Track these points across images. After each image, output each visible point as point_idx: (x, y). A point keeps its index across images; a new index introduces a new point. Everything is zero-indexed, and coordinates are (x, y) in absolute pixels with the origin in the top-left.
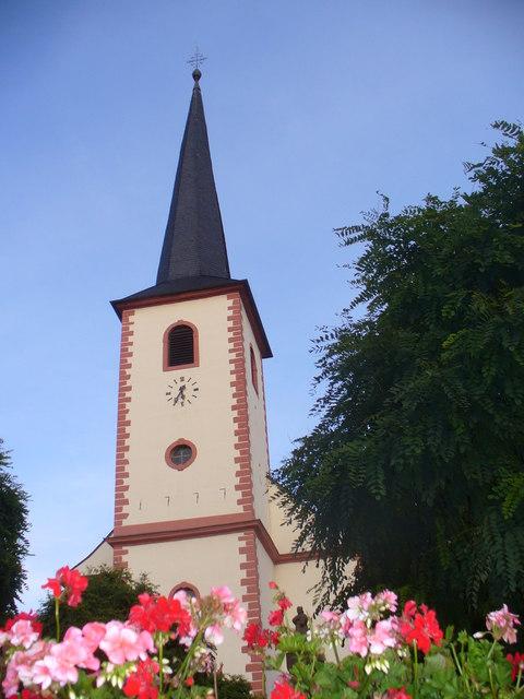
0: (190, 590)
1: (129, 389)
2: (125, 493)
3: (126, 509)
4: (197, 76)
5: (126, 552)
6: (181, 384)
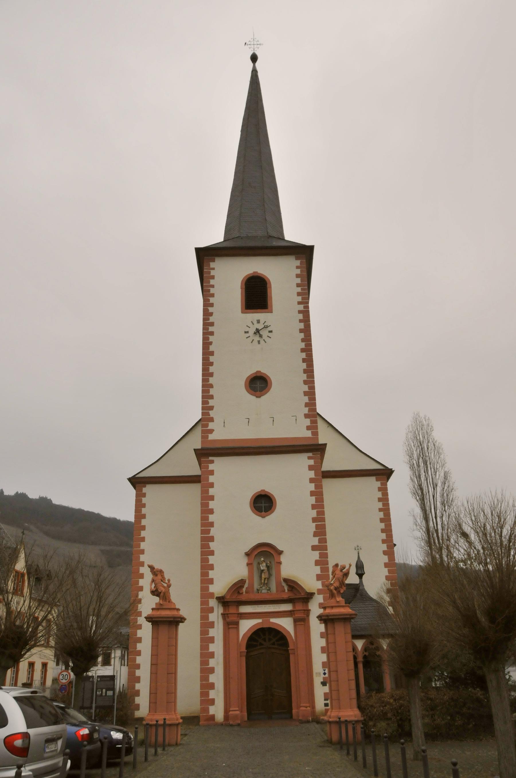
1: (212, 324)
4: (254, 58)
5: (212, 462)
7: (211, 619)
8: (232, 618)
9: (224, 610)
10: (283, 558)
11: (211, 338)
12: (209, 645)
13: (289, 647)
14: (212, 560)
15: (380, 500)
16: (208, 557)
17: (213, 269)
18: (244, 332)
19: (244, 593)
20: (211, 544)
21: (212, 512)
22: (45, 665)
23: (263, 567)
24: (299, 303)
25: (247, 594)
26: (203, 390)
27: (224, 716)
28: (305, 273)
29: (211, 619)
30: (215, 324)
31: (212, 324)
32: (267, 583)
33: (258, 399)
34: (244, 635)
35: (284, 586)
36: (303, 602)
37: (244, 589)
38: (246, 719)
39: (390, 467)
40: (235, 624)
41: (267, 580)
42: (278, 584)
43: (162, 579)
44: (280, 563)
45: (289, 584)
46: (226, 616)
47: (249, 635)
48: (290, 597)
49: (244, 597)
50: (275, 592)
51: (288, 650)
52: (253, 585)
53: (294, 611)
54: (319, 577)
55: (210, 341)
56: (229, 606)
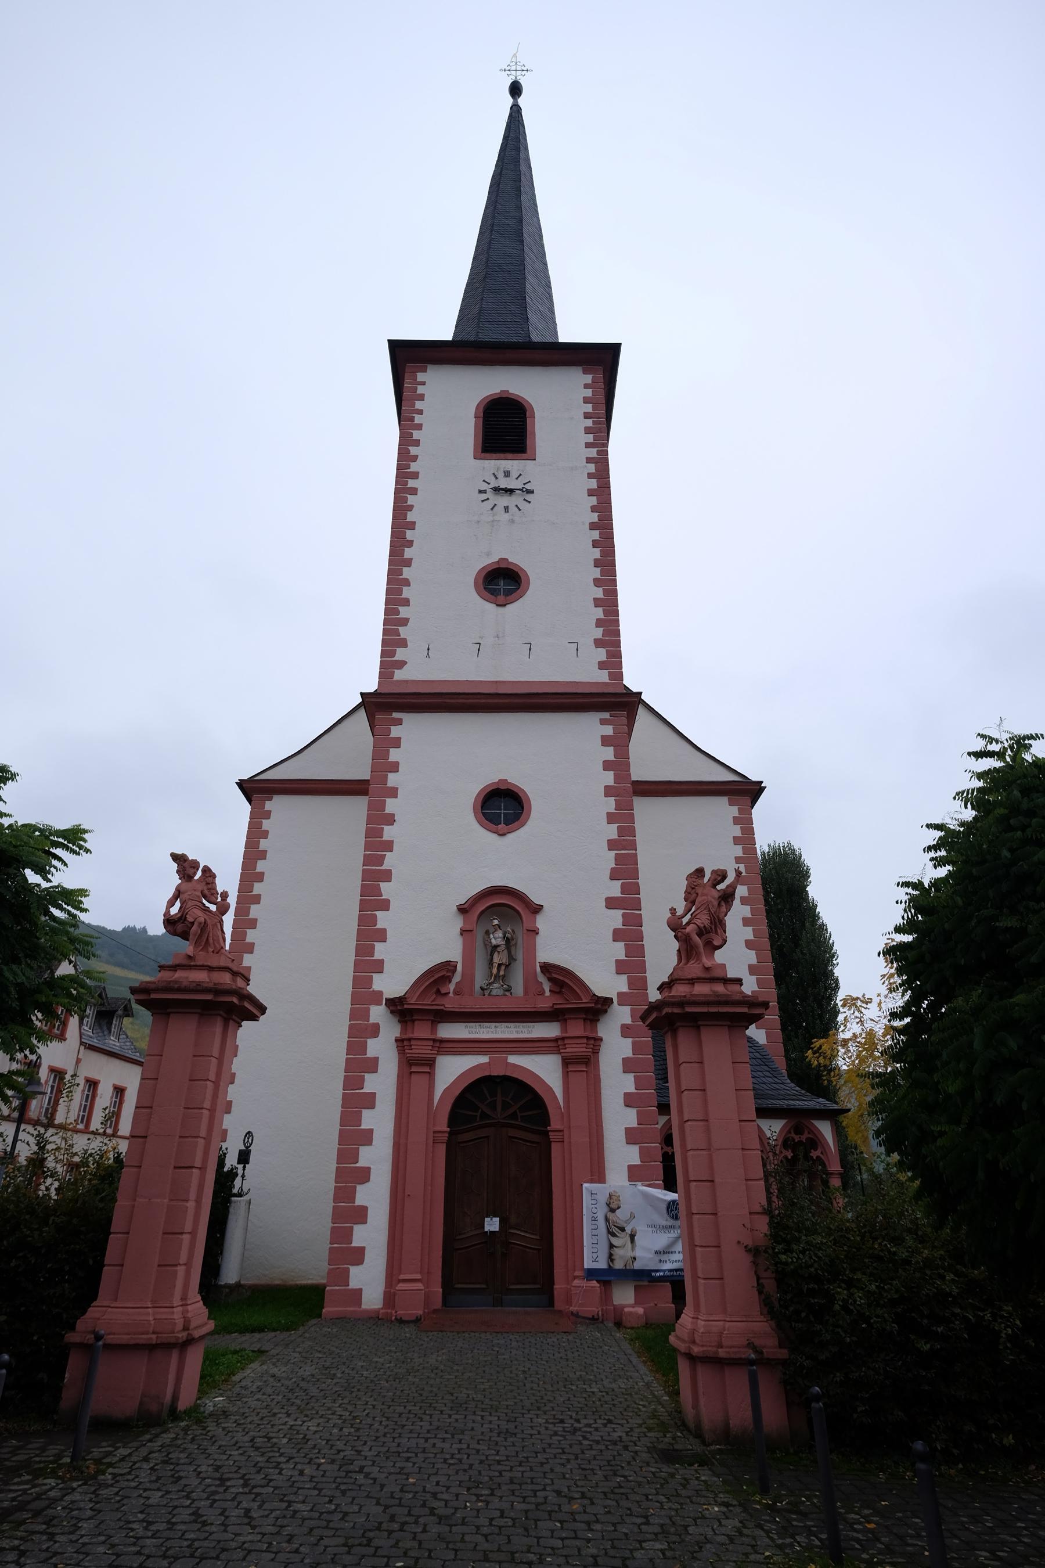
0: (105, 1109)
1: (415, 475)
2: (402, 630)
3: (400, 654)
4: (516, 90)
5: (399, 722)
6: (490, 494)
7: (371, 1053)
8: (419, 1050)
9: (404, 1030)
10: (541, 922)
11: (411, 499)
12: (361, 1112)
13: (550, 1126)
14: (383, 919)
15: (737, 841)
16: (375, 915)
17: (423, 383)
18: (477, 491)
19: (451, 994)
20: (383, 886)
21: (390, 820)
22: (119, 1091)
23: (497, 938)
24: (588, 445)
25: (457, 997)
26: (388, 590)
27: (385, 1293)
28: (602, 398)
29: (371, 1053)
30: (420, 476)
31: (415, 475)
32: (504, 976)
33: (501, 610)
34: (446, 1091)
35: (541, 983)
36: (585, 1020)
37: (452, 987)
38: (438, 1303)
39: (754, 777)
40: (427, 1065)
41: (505, 970)
42: (530, 980)
43: (206, 892)
44: (535, 932)
45: (554, 975)
46: (406, 1043)
47: (457, 1092)
48: (555, 1007)
49: (450, 1003)
50: (522, 995)
51: (546, 1134)
52: (473, 975)
53: (563, 1039)
54: (621, 967)
55: (409, 503)
56: (413, 1021)
